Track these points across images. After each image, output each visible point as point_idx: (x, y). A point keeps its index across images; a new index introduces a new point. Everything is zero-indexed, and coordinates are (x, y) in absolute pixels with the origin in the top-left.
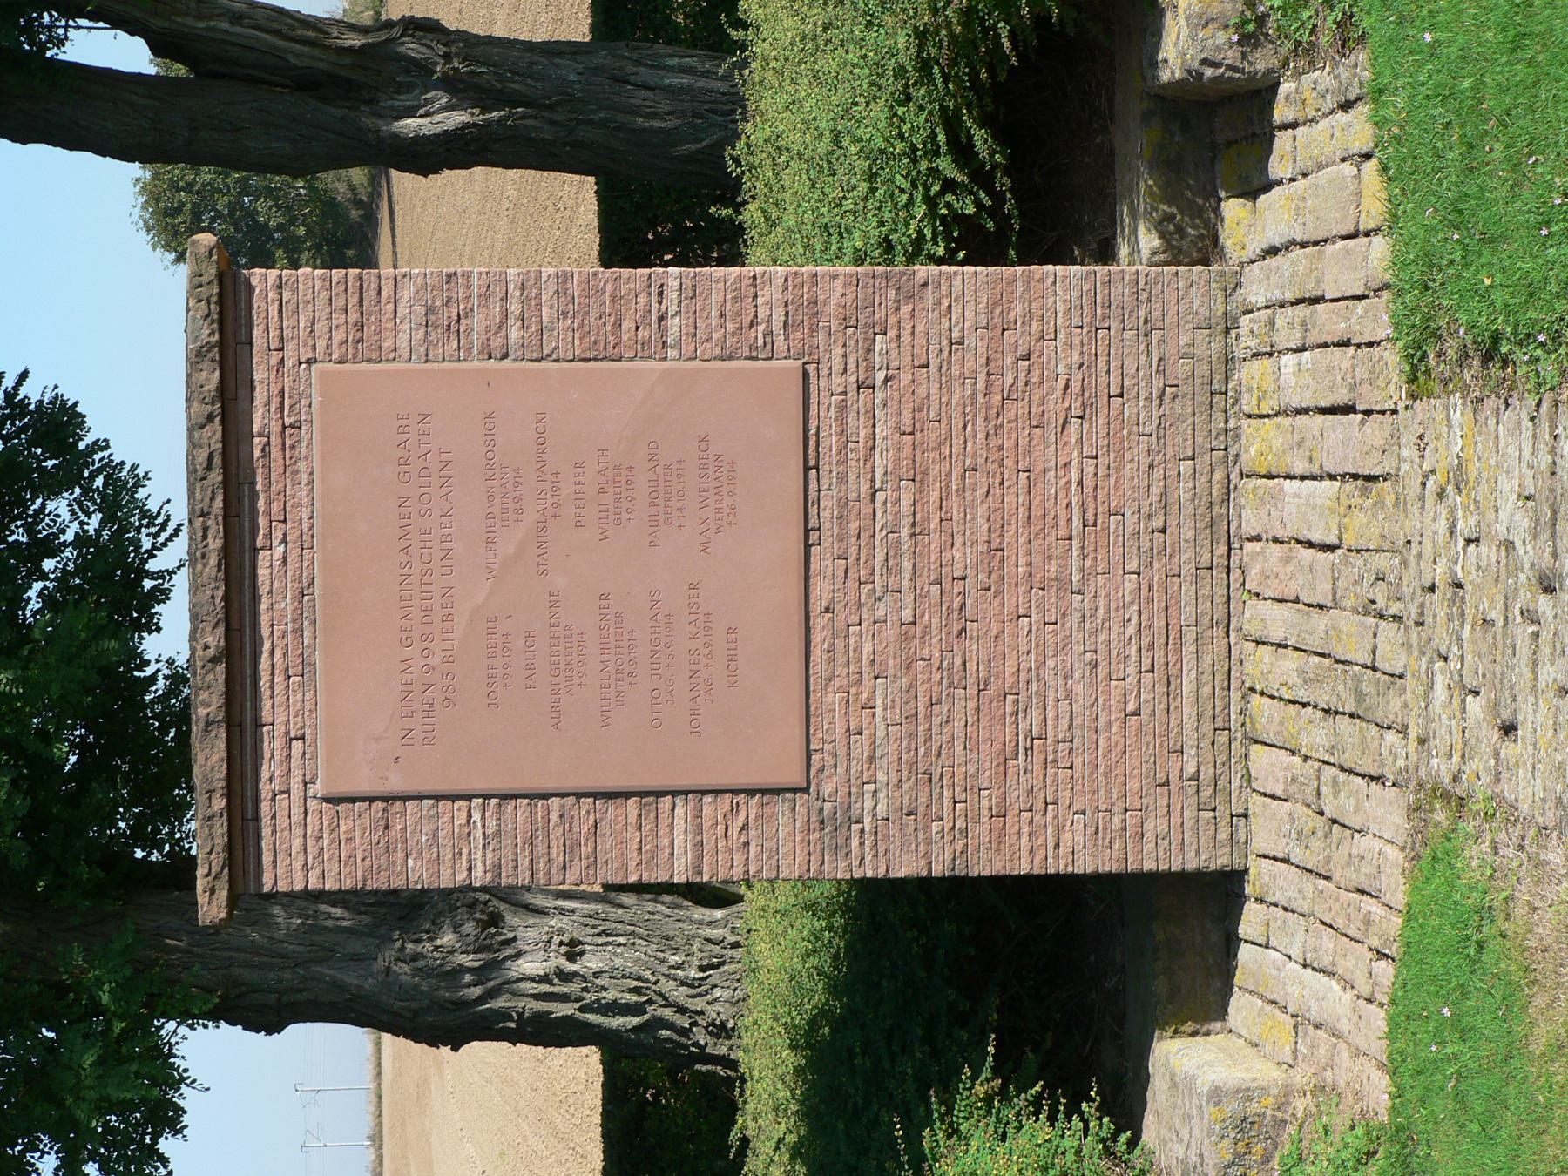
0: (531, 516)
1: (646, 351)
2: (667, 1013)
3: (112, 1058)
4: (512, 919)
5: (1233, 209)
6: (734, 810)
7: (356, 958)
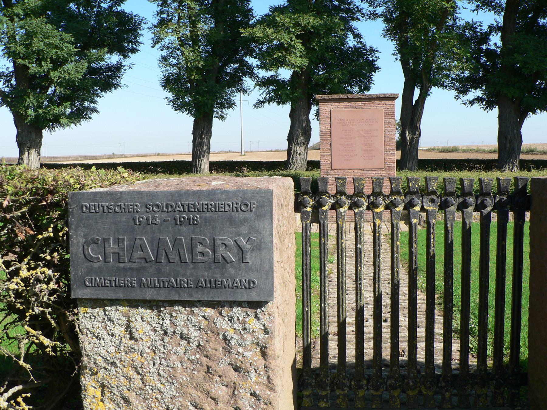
0: (365, 135)
1: (386, 149)
2: (292, 166)
3: (288, 95)
4: (304, 147)
5: (403, 222)
6: (329, 160)
7: (299, 127)
